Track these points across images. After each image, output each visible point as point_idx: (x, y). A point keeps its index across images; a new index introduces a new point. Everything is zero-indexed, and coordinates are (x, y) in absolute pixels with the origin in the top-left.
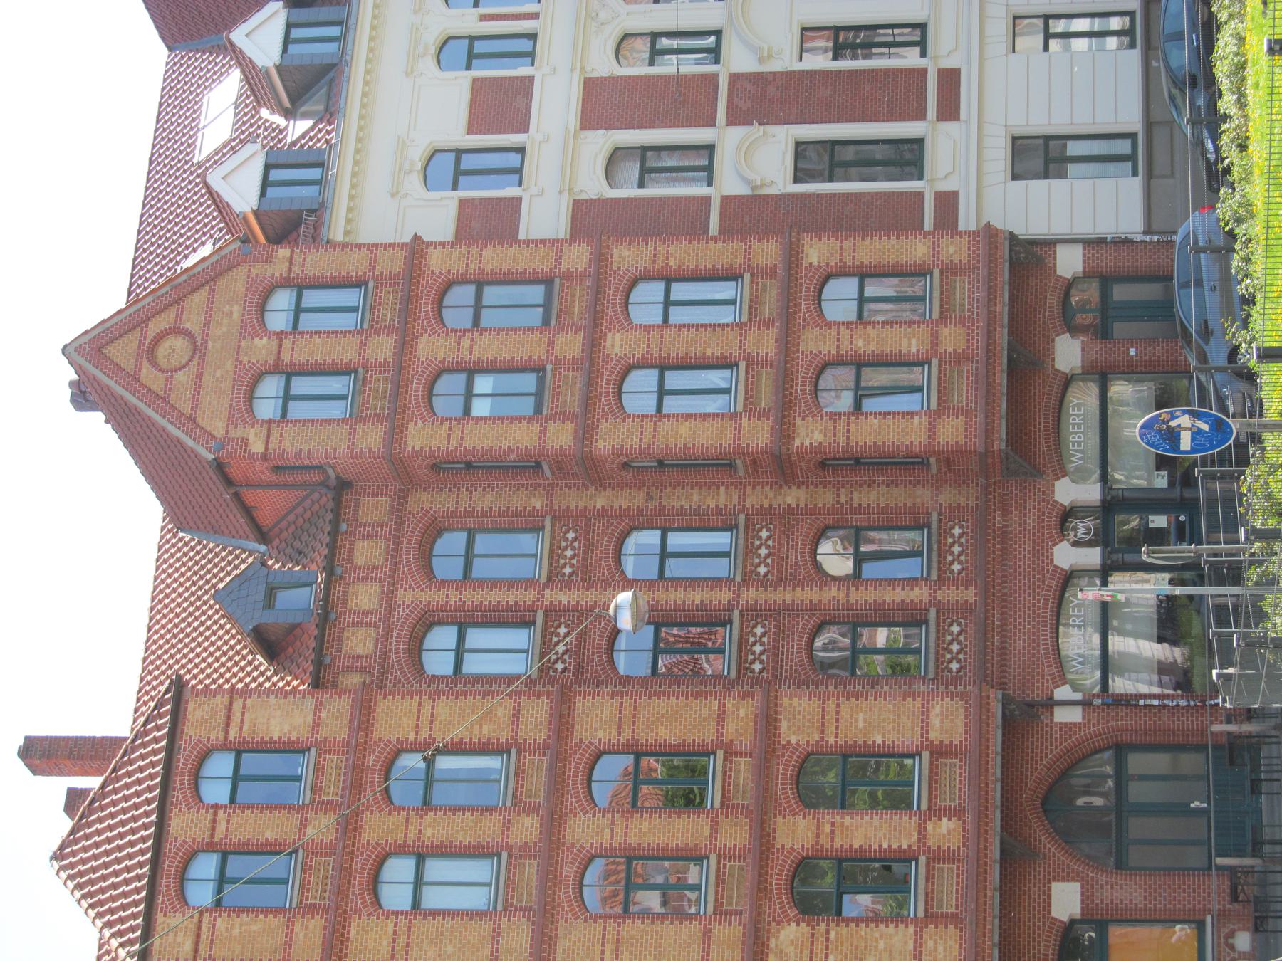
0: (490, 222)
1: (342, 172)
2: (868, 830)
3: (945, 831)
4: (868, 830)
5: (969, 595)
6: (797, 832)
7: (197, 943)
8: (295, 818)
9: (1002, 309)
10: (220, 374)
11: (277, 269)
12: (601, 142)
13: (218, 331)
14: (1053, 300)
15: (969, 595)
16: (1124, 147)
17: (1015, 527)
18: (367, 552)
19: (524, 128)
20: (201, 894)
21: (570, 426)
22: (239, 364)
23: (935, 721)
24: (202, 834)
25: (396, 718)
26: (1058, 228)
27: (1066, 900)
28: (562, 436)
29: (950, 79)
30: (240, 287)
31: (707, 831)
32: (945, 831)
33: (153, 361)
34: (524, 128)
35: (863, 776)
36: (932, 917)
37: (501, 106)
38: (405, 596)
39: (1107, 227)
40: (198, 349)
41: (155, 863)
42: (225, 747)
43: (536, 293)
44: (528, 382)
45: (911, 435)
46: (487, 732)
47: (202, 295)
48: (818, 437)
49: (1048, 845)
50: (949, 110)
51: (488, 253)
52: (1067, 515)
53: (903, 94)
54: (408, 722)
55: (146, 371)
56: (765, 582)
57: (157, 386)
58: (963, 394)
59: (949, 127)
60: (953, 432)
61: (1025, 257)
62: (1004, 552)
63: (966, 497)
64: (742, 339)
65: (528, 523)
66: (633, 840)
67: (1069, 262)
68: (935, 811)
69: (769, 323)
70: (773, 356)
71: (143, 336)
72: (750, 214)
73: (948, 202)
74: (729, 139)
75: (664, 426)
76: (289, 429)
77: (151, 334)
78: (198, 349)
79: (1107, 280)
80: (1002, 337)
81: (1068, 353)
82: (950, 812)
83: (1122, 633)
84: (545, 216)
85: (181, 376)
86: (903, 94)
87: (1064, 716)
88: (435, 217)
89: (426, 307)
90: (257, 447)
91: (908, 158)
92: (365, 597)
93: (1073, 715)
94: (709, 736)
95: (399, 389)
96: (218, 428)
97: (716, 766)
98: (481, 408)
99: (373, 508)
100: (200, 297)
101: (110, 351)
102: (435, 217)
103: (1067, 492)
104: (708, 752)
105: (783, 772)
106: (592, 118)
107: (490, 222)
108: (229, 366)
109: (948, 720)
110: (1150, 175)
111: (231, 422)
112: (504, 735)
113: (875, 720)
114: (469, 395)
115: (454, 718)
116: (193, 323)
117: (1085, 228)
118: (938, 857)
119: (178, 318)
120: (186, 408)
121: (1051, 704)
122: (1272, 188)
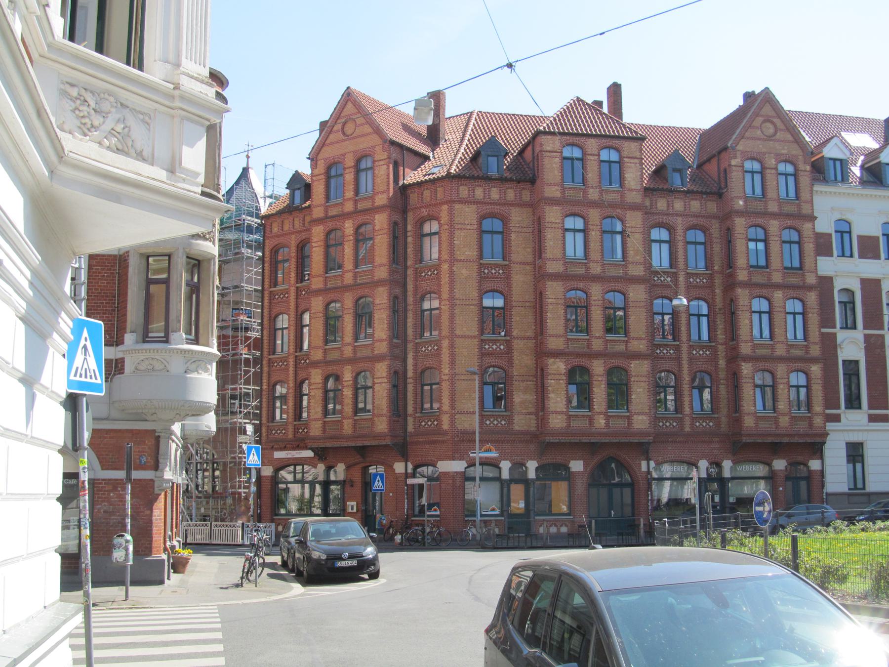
0: (823, 246)
1: (841, 188)
2: (600, 393)
3: (600, 422)
4: (600, 393)
6: (598, 368)
7: (549, 152)
9: (796, 440)
11: (801, 166)
15: (687, 429)
16: (860, 485)
17: (713, 446)
19: (861, 257)
21: (746, 279)
22: (764, 154)
23: (640, 417)
24: (589, 151)
25: (635, 220)
26: (827, 461)
27: (577, 466)
28: (742, 276)
30: (794, 152)
31: (597, 335)
32: (600, 422)
33: (764, 121)
34: (861, 257)
35: (619, 392)
37: (868, 248)
38: (679, 220)
40: (770, 138)
42: (621, 157)
43: (796, 264)
44: (762, 262)
46: (631, 253)
48: (745, 372)
50: (873, 419)
51: (811, 245)
52: (718, 465)
54: (633, 224)
55: (761, 119)
56: (690, 353)
57: (755, 124)
58: (764, 426)
59: (865, 419)
60: (749, 422)
62: (703, 442)
63: (724, 427)
64: (782, 342)
66: (593, 308)
67: (815, 465)
68: (608, 418)
71: (774, 117)
72: (830, 344)
73: (837, 419)
74: (859, 334)
75: (748, 314)
76: (741, 174)
77: (775, 120)
78: (770, 138)
80: (785, 440)
81: (780, 464)
82: (607, 425)
83: (671, 486)
84: (826, 266)
85: (759, 132)
87: (644, 464)
88: (825, 224)
89: (789, 223)
90: (733, 162)
91: (853, 402)
92: (678, 205)
93: (644, 467)
98: (752, 245)
100: (789, 137)
102: (825, 224)
103: (727, 465)
104: (626, 334)
105: (620, 362)
108: (764, 150)
111: (743, 152)
112: (630, 259)
113: (640, 394)
114: (756, 240)
115: (636, 241)
116: (779, 135)
117: (828, 471)
119: (781, 130)
120: (747, 134)
121: (648, 460)
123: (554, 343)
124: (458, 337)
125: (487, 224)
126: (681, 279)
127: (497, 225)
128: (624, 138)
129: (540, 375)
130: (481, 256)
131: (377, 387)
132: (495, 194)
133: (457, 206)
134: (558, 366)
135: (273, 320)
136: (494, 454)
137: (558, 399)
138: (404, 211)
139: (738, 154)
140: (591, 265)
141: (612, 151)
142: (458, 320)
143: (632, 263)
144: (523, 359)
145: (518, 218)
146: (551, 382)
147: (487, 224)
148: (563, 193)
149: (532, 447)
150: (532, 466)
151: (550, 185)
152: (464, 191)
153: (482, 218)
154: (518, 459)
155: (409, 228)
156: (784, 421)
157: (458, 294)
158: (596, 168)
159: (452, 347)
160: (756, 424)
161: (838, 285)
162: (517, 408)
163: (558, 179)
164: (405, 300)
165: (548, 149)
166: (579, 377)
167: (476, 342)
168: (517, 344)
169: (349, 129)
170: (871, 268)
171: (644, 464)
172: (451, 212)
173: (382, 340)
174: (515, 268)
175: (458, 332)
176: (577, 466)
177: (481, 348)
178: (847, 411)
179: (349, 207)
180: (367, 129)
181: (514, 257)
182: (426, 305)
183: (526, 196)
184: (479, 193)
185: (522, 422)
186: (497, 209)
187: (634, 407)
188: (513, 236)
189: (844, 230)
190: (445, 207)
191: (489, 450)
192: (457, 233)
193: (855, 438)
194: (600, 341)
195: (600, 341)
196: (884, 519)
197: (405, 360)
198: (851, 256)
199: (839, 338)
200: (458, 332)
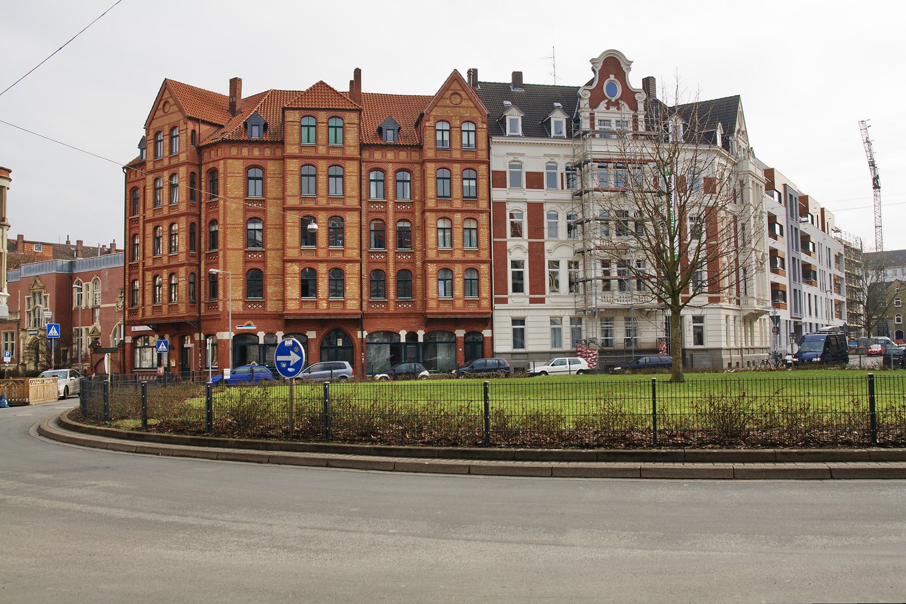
0: (499, 180)
2: (323, 286)
3: (323, 305)
5: (392, 309)
6: (322, 269)
8: (325, 143)
9: (467, 316)
10: (449, 112)
11: (480, 125)
12: (524, 207)
13: (462, 111)
14: (476, 329)
15: (392, 309)
17: (410, 320)
18: (403, 155)
20: (305, 122)
23: (352, 302)
24: (320, 120)
25: (352, 168)
26: (496, 330)
28: (431, 204)
29: (542, 301)
32: (323, 305)
33: (453, 94)
36: (246, 303)
38: (390, 165)
39: (496, 342)
40: (456, 106)
41: (310, 109)
42: (317, 123)
43: (447, 194)
44: (473, 194)
45: (432, 293)
46: (348, 190)
47: (473, 105)
48: (430, 270)
49: (324, 331)
50: (532, 301)
53: (537, 287)
54: (351, 169)
55: (450, 92)
56: (395, 258)
59: (528, 300)
60: (432, 304)
61: (488, 322)
65: (412, 195)
67: (487, 333)
68: (329, 302)
69: (464, 256)
70: (120, 246)
72: (501, 250)
73: (505, 301)
74: (524, 241)
75: (434, 230)
76: (433, 132)
78: (456, 106)
79: (482, 343)
80: (460, 316)
81: (460, 333)
82: (328, 308)
84: (498, 194)
85: (448, 102)
86: (537, 287)
87: (359, 333)
88: (498, 164)
89: (468, 165)
90: (427, 124)
91: (518, 288)
92: (390, 155)
93: (359, 336)
94: (348, 246)
95: (443, 161)
96: (433, 113)
97: (340, 248)
98: (466, 183)
99: (415, 156)
101: (455, 82)
102: (498, 164)
103: (280, 334)
104: (343, 244)
105: (338, 265)
106: (530, 205)
107: (499, 180)
109: (352, 305)
110: (512, 354)
111: (435, 116)
112: (347, 194)
113: (352, 287)
114: (469, 179)
115: (352, 181)
116: (463, 103)
117: (496, 337)
118: (264, 303)
121: (362, 330)
122: (846, 381)
123: (292, 253)
124: (230, 249)
125: (252, 173)
126: (391, 206)
127: (259, 173)
128: (346, 110)
129: (283, 273)
130: (247, 195)
131: (180, 284)
132: (256, 152)
133: (229, 161)
134: (295, 268)
135: (679, 225)
136: (253, 328)
137: (293, 291)
138: (200, 166)
139: (431, 118)
140: (319, 199)
141: (338, 120)
142: (229, 238)
143: (349, 197)
144: (272, 265)
145: (272, 167)
146: (288, 279)
147: (252, 173)
148: (300, 150)
149: (280, 322)
150: (421, 334)
151: (291, 144)
152: (234, 151)
153: (248, 168)
154: (270, 330)
155: (203, 176)
156: (459, 303)
157: (229, 220)
158: (325, 132)
159: (224, 256)
160: (438, 306)
161: (510, 208)
162: (269, 296)
163: (297, 141)
164: (200, 226)
165: (290, 119)
166: (446, 272)
167: (241, 252)
168: (270, 254)
169: (167, 109)
170: (535, 195)
171: (359, 333)
172: (225, 164)
173: (182, 253)
174: (269, 202)
175: (229, 246)
176: (312, 335)
177: (245, 257)
178: (515, 294)
179: (166, 162)
180: (175, 108)
181: (269, 195)
182: (309, 227)
183: (278, 153)
184: (245, 152)
185: (272, 306)
186: (257, 162)
187: (320, 295)
188: (269, 180)
189: (516, 165)
190: (222, 162)
191: (249, 325)
192: (229, 179)
193: (518, 314)
194: (325, 251)
195: (325, 251)
196: (903, 367)
197: (199, 266)
198: (562, 188)
199: (510, 245)
200: (229, 246)
